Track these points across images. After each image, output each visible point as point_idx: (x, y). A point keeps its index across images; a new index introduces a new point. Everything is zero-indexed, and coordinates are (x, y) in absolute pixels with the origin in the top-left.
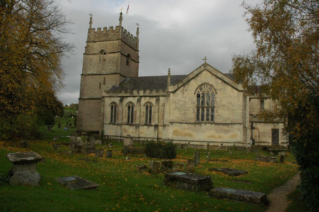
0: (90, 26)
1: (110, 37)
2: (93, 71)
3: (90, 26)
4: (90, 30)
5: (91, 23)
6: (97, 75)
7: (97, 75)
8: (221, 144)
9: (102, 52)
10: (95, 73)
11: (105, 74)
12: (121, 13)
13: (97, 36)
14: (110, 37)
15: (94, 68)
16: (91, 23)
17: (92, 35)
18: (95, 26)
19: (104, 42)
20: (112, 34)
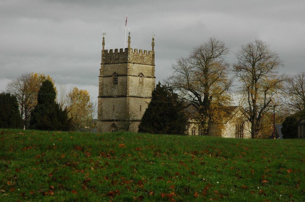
0: (103, 47)
1: (145, 61)
2: (134, 93)
3: (103, 47)
4: (105, 52)
5: (103, 44)
6: (137, 97)
7: (137, 97)
8: (13, 173)
9: (141, 75)
10: (135, 95)
11: (145, 98)
12: (153, 38)
13: (135, 57)
14: (145, 61)
15: (135, 90)
16: (103, 44)
17: (131, 55)
18: (108, 47)
19: (141, 65)
20: (147, 58)
